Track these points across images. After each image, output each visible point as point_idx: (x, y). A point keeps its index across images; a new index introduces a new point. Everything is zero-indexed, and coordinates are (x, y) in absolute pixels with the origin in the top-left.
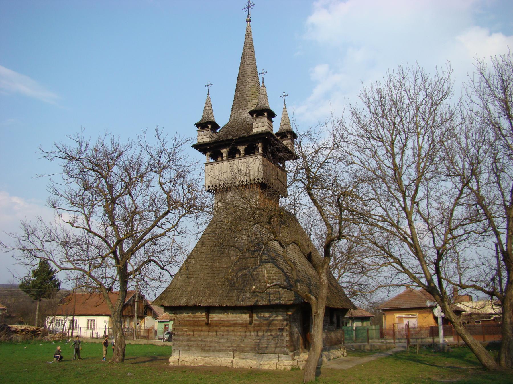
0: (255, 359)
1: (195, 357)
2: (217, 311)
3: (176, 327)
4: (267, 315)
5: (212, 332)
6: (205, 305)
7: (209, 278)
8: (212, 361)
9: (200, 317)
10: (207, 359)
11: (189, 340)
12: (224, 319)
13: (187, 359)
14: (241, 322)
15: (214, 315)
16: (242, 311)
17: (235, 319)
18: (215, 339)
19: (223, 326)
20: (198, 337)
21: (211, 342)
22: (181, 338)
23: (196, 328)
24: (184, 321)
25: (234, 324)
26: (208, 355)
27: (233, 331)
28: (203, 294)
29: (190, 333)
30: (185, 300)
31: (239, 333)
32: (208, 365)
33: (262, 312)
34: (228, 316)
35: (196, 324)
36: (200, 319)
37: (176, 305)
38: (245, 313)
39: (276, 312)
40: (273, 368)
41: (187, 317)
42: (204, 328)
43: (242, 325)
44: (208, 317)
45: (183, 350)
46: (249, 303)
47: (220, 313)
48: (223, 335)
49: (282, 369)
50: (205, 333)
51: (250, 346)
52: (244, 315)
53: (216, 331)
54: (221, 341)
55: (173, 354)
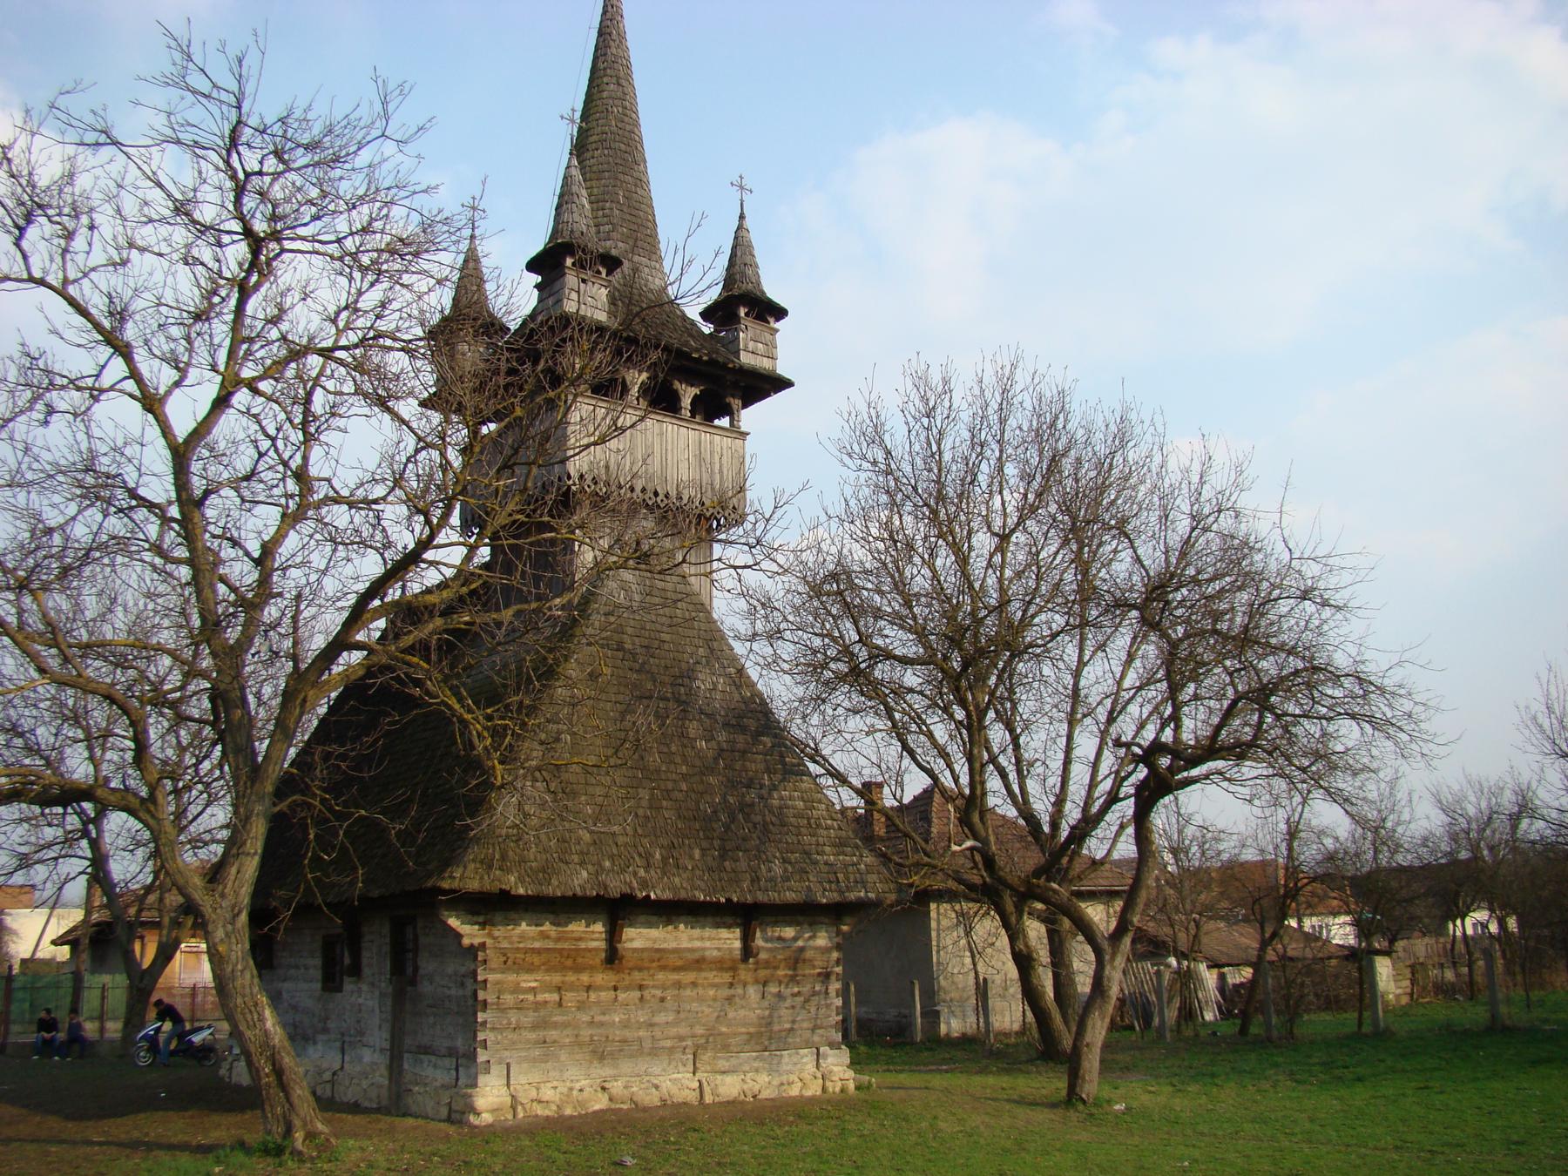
9: (580, 939)
23: (571, 977)
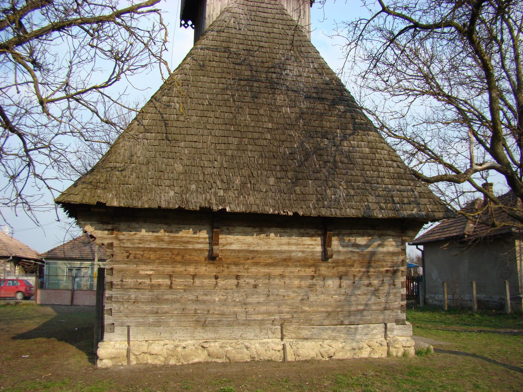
0: (334, 339)
1: (177, 343)
2: (239, 229)
3: (116, 266)
4: (362, 241)
5: (226, 278)
6: (238, 210)
7: (231, 147)
8: (230, 348)
9: (188, 242)
10: (214, 346)
11: (157, 300)
12: (258, 248)
13: (156, 348)
14: (300, 254)
15: (231, 238)
16: (302, 231)
17: (285, 248)
18: (236, 295)
19: (257, 264)
20: (185, 290)
21: (224, 303)
22: (133, 295)
23: (180, 268)
24: (144, 249)
25: (285, 260)
26: (213, 336)
27: (282, 276)
28: (222, 181)
29: (161, 281)
30: (172, 193)
31: (296, 282)
32: (218, 360)
33: (350, 235)
34: (270, 240)
35: (179, 258)
36: (190, 246)
37: (146, 206)
38: (312, 236)
39: (380, 236)
40: (380, 353)
41: (150, 241)
42: (203, 269)
43: (303, 262)
44: (213, 241)
45: (138, 325)
46: (351, 213)
47: (246, 234)
48: (255, 286)
49: (400, 354)
50: (206, 281)
51: (323, 309)
52: (307, 240)
53: (237, 277)
54: (249, 300)
55: (106, 336)
